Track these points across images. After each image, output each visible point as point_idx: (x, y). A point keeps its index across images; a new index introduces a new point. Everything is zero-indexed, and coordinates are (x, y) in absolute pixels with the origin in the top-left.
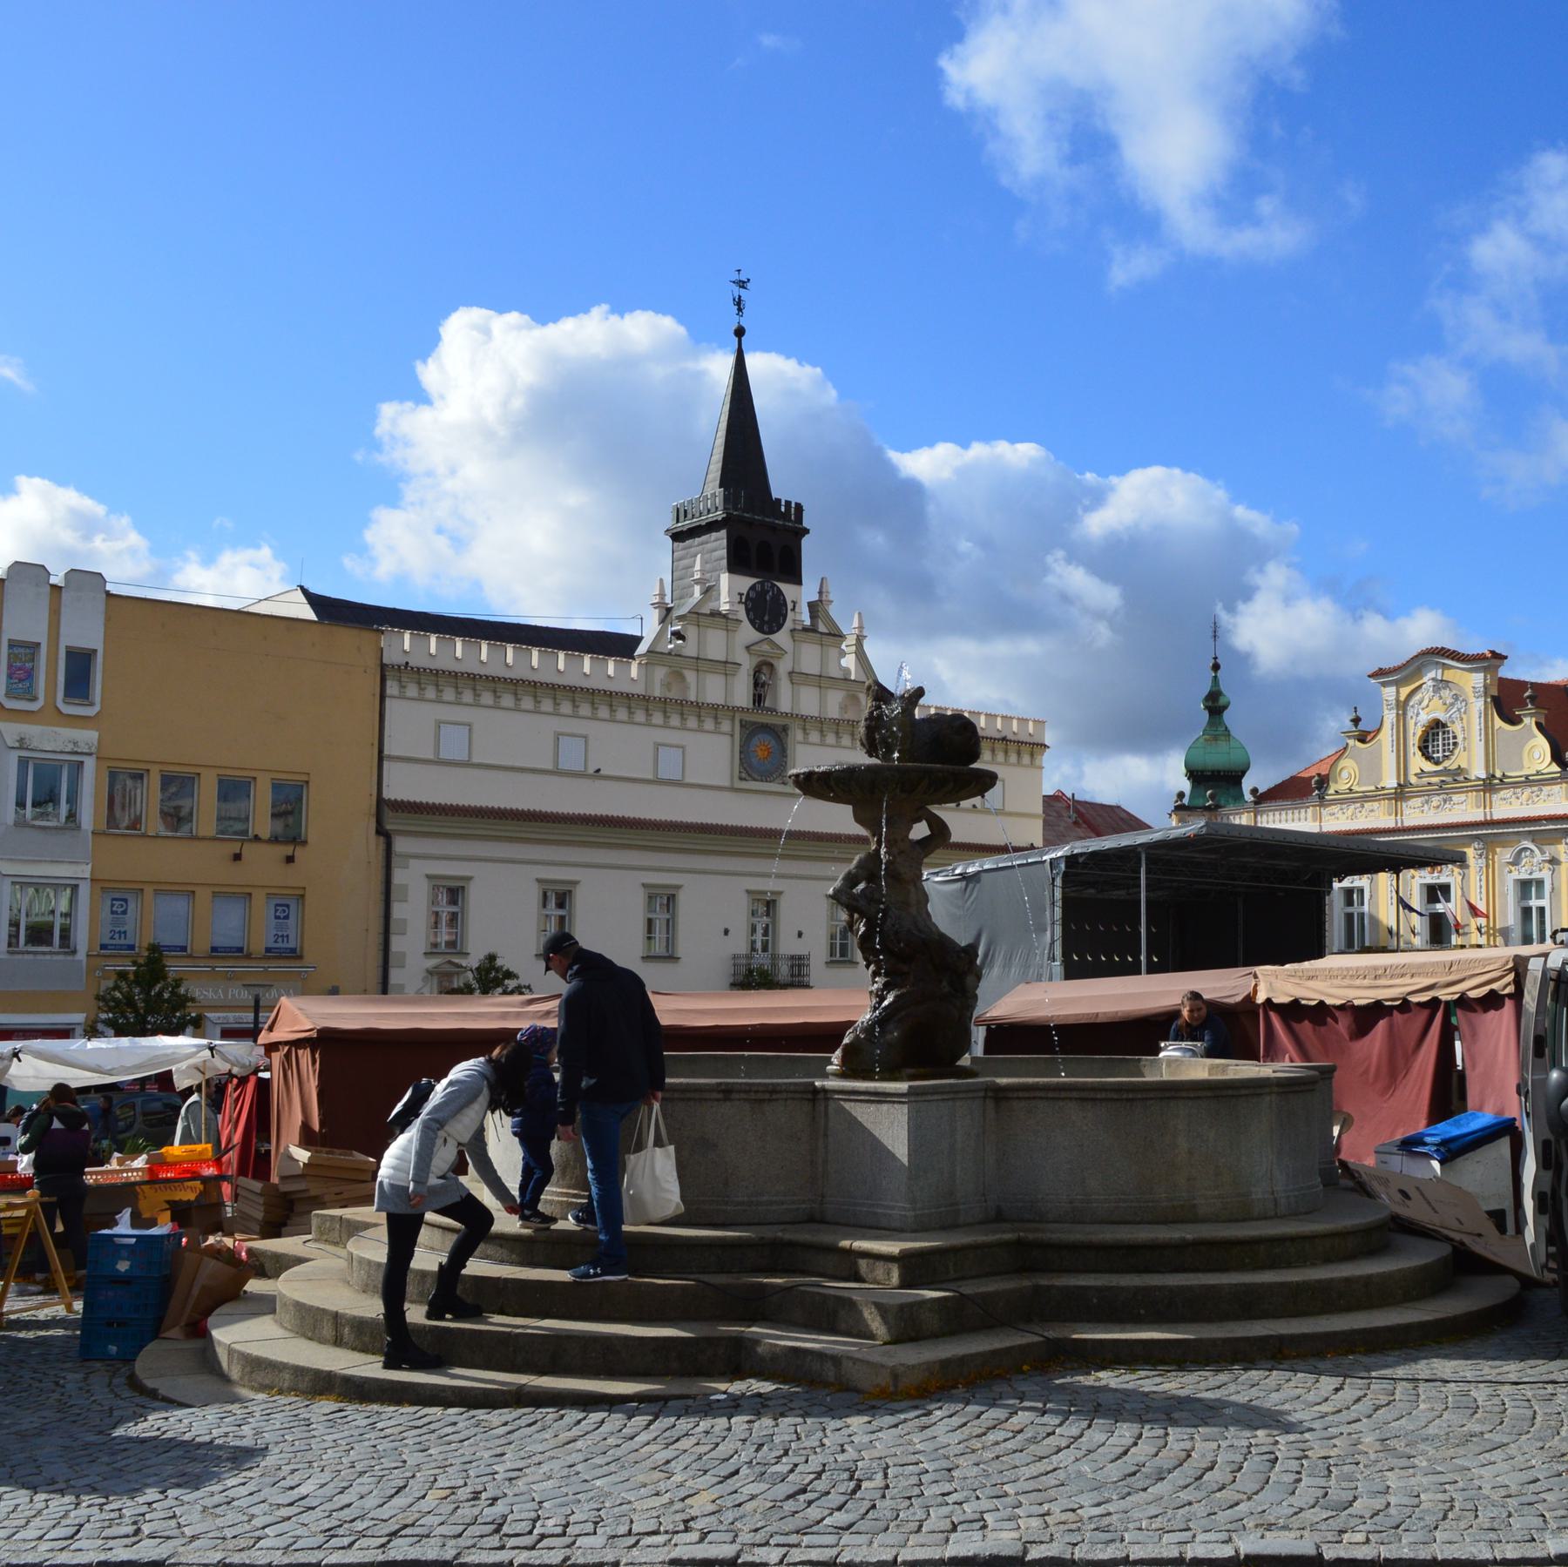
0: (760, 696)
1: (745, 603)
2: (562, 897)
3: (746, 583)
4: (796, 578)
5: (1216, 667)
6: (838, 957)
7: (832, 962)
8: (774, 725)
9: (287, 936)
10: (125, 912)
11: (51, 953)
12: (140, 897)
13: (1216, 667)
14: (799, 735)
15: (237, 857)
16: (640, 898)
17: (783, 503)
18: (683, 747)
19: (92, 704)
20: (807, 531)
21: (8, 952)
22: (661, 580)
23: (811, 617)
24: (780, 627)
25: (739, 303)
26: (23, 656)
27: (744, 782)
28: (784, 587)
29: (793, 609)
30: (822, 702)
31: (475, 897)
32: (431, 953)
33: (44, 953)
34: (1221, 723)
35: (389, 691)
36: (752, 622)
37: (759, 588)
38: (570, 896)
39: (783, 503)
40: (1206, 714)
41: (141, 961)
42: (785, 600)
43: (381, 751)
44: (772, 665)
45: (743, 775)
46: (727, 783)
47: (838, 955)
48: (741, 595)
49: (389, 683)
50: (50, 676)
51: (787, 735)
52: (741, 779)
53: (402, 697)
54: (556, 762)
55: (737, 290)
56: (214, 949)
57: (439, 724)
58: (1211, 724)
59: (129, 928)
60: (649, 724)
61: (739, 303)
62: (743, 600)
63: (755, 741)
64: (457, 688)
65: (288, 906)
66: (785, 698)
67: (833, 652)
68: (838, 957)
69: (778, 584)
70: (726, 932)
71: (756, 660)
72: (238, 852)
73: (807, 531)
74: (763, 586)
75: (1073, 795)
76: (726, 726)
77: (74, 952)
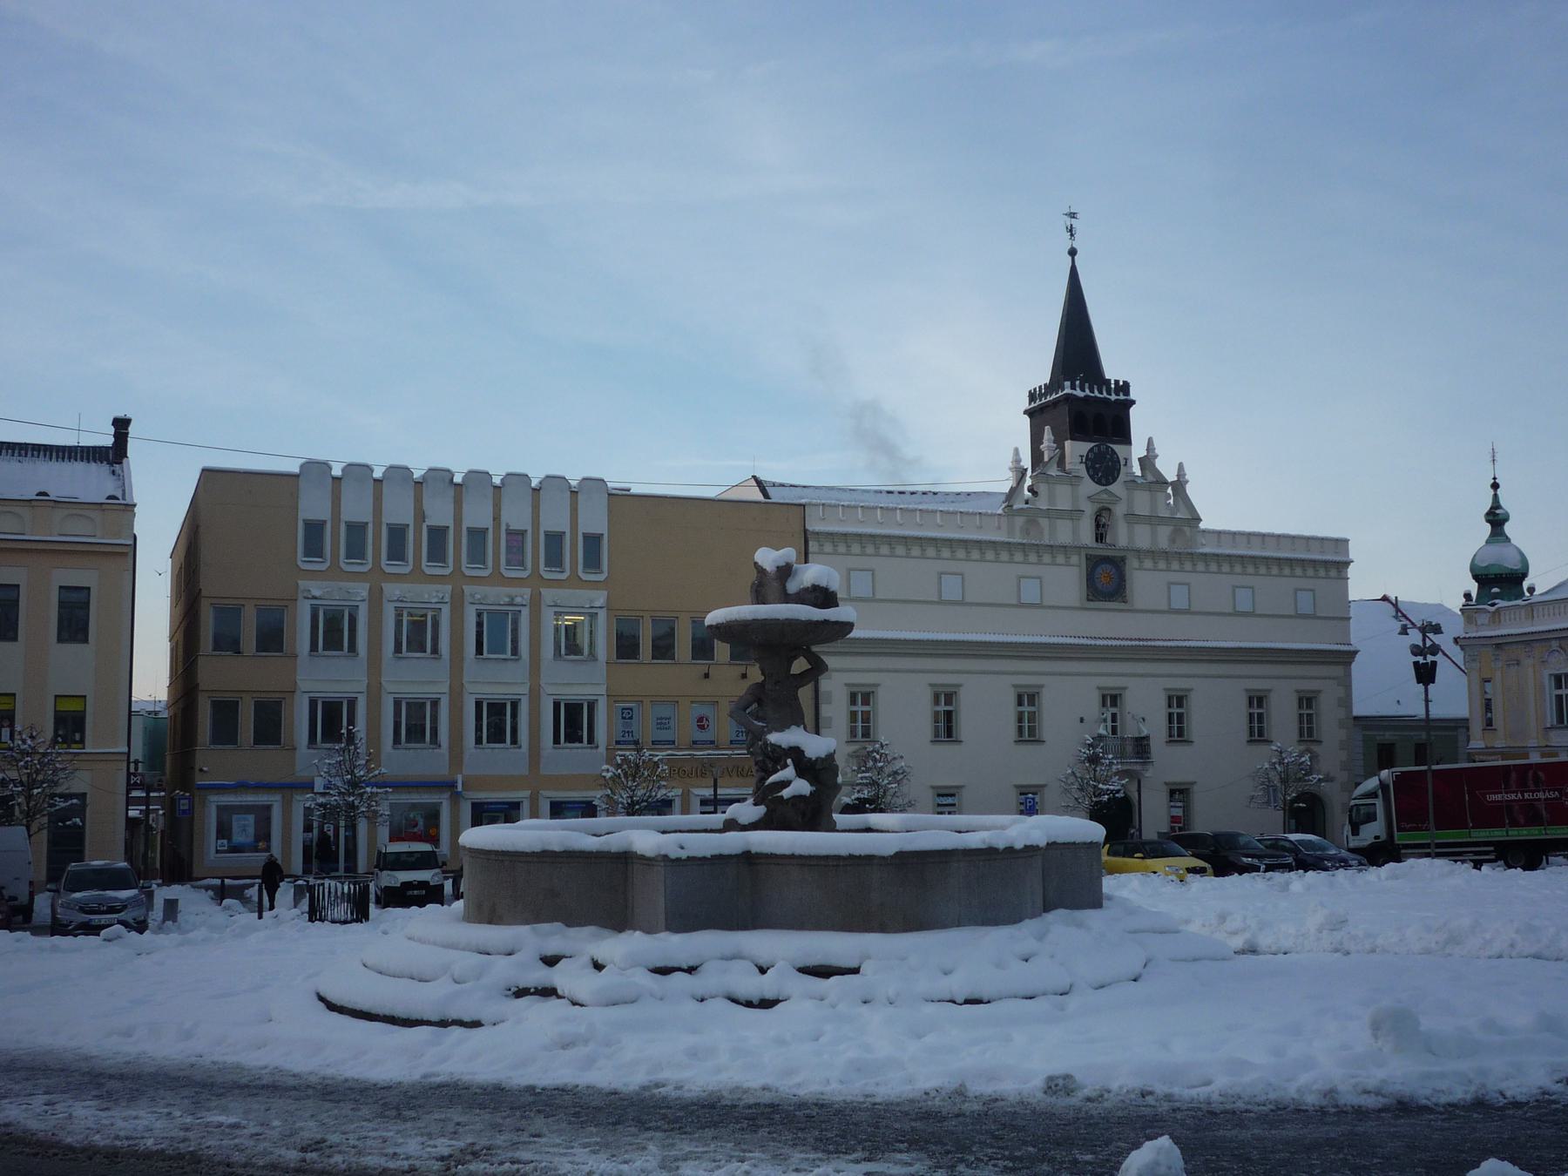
0: (1102, 534)
1: (1086, 463)
2: (1112, 699)
3: (1084, 447)
4: (1125, 438)
5: (1495, 486)
6: (1256, 737)
7: (1170, 741)
8: (1115, 557)
9: (632, 732)
10: (631, 718)
11: (582, 748)
12: (716, 707)
13: (1495, 486)
14: (1135, 564)
15: (707, 676)
16: (927, 697)
17: (1113, 382)
18: (962, 574)
19: (602, 572)
20: (1133, 402)
21: (476, 748)
22: (1016, 451)
23: (1141, 469)
24: (1115, 480)
25: (1071, 231)
26: (314, 530)
27: (1092, 603)
28: (1116, 448)
29: (1126, 465)
30: (1075, 532)
31: (1047, 700)
32: (1020, 741)
33: (578, 748)
34: (1502, 534)
35: (811, 549)
36: (1092, 477)
37: (1096, 450)
38: (1186, 699)
39: (1113, 382)
40: (1488, 527)
41: (776, 755)
42: (1118, 458)
43: (1230, 614)
44: (1109, 510)
45: (1090, 597)
46: (1077, 604)
47: (1306, 735)
48: (1082, 456)
49: (811, 543)
50: (574, 552)
51: (1125, 564)
52: (1088, 600)
53: (821, 552)
54: (1019, 596)
55: (1069, 221)
56: (695, 742)
57: (1020, 578)
58: (1493, 534)
59: (634, 728)
60: (1011, 562)
61: (1071, 231)
62: (1084, 461)
63: (1099, 570)
64: (1038, 553)
65: (631, 709)
66: (1121, 536)
67: (1160, 495)
68: (1256, 737)
69: (1111, 446)
70: (1082, 720)
71: (1097, 506)
72: (707, 672)
73: (1133, 402)
74: (1099, 449)
75: (1396, 598)
76: (1074, 559)
77: (520, 747)
